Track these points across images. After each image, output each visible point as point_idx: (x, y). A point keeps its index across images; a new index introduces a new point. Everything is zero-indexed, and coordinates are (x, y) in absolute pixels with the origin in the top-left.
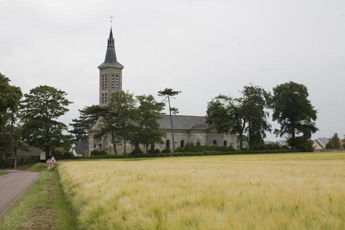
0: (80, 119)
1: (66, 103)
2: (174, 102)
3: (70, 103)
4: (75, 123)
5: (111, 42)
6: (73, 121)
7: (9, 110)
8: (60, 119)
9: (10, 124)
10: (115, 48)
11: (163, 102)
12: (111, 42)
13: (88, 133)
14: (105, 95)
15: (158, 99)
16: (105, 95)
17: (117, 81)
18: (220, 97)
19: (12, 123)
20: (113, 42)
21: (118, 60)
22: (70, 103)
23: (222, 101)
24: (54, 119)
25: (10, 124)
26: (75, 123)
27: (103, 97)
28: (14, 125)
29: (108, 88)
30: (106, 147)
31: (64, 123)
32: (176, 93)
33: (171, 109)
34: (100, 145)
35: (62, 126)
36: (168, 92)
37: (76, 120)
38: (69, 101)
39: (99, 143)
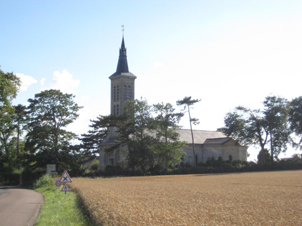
0: (89, 134)
1: (75, 108)
2: (194, 110)
3: (80, 108)
4: (84, 137)
5: (123, 51)
6: (82, 135)
7: (15, 121)
8: (68, 128)
9: (16, 136)
10: (127, 58)
11: (182, 112)
12: (123, 51)
13: (96, 148)
14: (116, 107)
15: (178, 109)
16: (116, 107)
17: (129, 91)
18: (240, 108)
19: (18, 135)
20: (125, 50)
21: (130, 70)
22: (80, 108)
23: (239, 112)
24: (62, 128)
25: (16, 136)
26: (84, 137)
27: (114, 108)
28: (20, 138)
29: (120, 100)
30: (119, 162)
31: (73, 132)
32: (194, 101)
33: (192, 120)
34: (112, 160)
35: (71, 135)
36: (187, 101)
37: (85, 135)
38: (79, 106)
39: (111, 158)
